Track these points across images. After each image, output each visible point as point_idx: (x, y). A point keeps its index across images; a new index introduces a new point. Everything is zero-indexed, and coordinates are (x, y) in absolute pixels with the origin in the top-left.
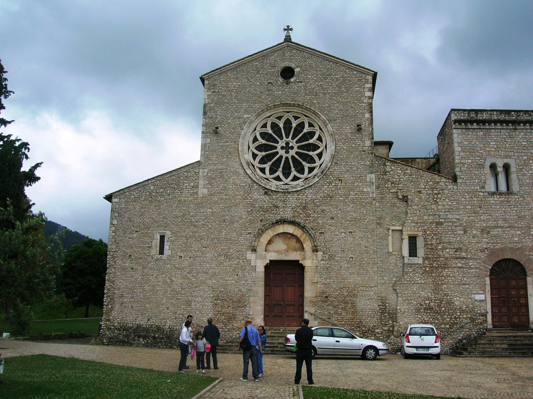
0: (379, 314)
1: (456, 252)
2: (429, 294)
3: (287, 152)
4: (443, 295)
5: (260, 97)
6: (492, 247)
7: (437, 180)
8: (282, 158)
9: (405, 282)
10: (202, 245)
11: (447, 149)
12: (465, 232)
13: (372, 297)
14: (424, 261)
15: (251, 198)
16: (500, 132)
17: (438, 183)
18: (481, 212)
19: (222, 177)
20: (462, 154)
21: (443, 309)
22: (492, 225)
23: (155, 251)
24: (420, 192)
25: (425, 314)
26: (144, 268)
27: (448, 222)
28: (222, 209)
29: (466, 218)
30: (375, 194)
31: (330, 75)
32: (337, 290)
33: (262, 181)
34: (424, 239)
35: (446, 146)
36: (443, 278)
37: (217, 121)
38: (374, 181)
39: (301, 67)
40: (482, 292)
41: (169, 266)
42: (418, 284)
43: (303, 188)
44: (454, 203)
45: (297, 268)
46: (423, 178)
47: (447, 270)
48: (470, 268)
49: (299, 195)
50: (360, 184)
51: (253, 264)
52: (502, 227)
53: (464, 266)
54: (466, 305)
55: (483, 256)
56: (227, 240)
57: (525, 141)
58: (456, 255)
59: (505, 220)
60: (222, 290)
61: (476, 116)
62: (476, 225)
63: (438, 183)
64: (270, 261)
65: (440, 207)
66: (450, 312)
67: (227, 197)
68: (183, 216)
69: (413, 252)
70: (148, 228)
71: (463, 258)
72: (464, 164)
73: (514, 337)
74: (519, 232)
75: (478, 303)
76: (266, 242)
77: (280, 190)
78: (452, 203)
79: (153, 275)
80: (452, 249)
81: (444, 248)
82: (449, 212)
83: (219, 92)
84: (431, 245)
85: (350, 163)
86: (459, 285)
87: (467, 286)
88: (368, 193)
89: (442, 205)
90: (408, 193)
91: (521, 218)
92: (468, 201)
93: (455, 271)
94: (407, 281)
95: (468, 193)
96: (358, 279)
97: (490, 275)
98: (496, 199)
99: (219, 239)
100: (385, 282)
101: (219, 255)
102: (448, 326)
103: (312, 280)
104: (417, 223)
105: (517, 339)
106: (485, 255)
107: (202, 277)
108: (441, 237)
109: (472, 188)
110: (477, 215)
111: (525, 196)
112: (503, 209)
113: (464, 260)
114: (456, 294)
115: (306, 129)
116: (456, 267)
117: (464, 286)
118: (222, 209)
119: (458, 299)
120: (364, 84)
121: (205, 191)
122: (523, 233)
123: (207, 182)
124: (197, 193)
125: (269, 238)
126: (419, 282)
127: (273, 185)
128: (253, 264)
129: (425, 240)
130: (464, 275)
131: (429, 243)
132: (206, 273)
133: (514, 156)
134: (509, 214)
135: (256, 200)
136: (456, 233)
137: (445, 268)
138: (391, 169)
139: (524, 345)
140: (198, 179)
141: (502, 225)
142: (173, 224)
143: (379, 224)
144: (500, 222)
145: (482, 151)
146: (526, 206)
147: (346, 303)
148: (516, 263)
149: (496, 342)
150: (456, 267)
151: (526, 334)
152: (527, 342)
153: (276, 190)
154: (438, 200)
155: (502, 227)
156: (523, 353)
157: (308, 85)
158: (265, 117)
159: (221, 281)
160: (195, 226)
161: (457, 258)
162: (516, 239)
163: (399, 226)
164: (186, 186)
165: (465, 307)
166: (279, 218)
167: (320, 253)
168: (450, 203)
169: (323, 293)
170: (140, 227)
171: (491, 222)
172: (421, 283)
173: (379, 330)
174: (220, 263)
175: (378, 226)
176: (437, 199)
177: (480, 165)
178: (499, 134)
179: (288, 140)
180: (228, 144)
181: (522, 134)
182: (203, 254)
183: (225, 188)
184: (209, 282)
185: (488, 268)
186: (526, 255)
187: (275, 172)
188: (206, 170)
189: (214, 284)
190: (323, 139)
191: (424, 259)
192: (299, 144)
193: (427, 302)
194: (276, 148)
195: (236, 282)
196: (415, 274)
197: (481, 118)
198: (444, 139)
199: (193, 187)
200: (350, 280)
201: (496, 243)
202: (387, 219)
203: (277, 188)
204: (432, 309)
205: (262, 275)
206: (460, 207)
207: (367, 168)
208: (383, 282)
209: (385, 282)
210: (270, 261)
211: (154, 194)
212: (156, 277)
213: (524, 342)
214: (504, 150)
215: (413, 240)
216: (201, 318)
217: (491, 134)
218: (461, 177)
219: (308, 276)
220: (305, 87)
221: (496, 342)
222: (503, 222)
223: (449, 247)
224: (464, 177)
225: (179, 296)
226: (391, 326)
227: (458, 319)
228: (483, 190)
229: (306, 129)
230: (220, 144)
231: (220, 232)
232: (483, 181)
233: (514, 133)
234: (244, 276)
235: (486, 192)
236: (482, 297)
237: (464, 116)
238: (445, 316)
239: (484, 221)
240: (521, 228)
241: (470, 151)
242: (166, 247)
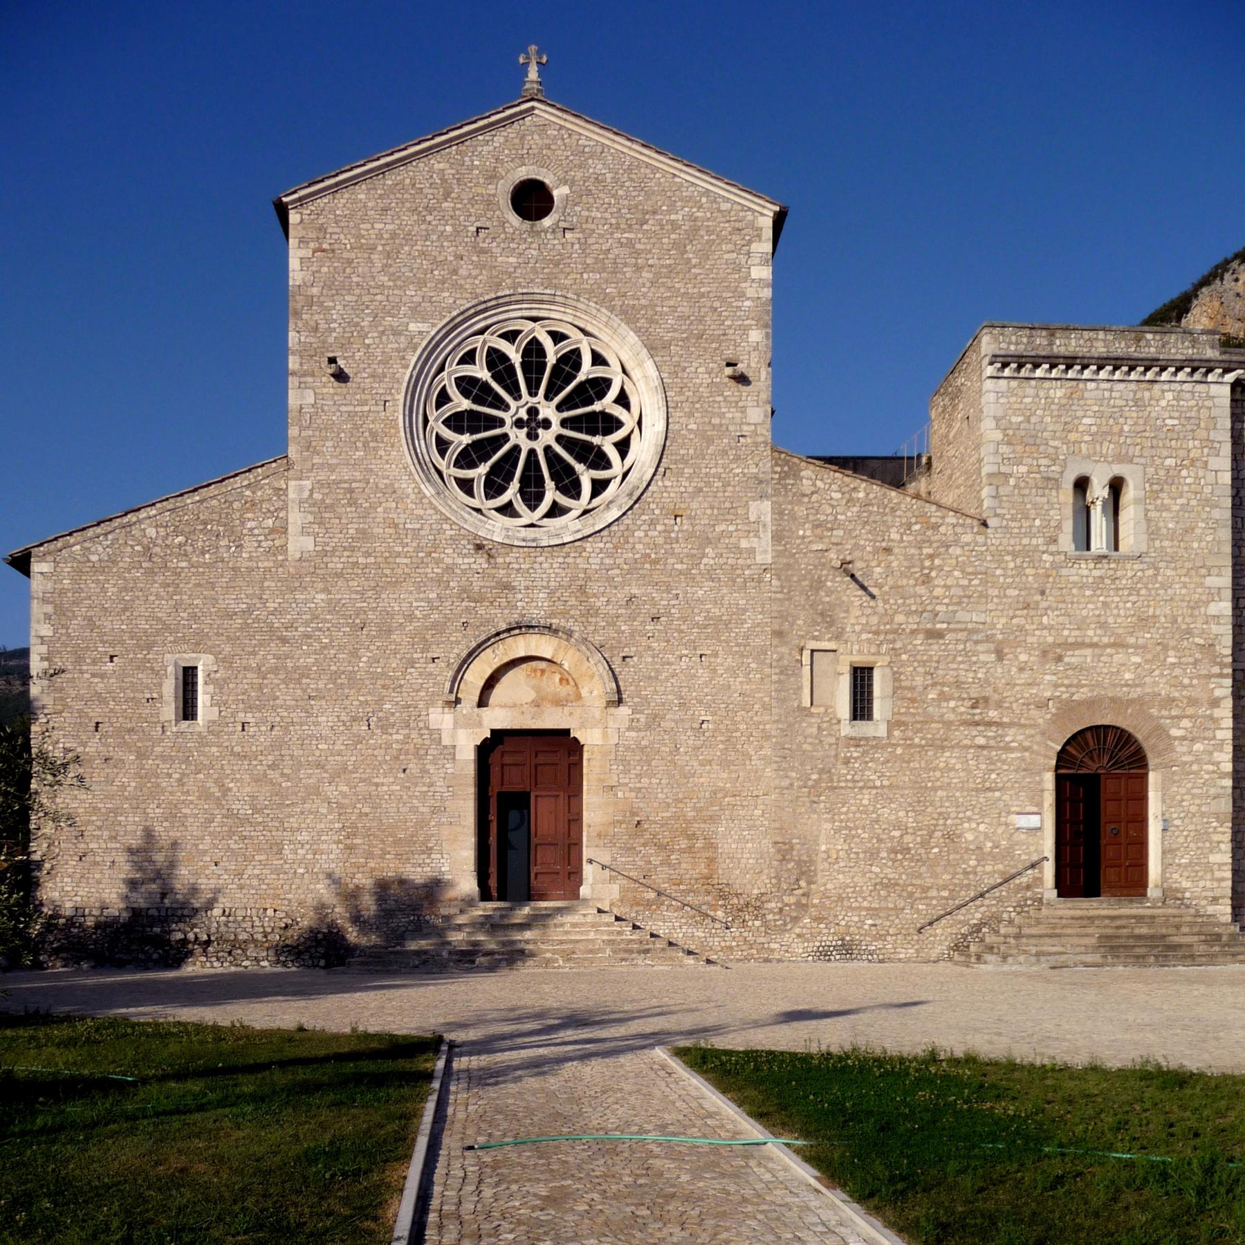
0: (775, 863)
1: (973, 707)
2: (901, 814)
3: (532, 436)
4: (936, 816)
5: (455, 272)
6: (1064, 696)
7: (933, 520)
8: (536, 455)
9: (843, 784)
10: (304, 691)
11: (960, 432)
12: (1000, 656)
13: (758, 823)
14: (889, 732)
15: (438, 562)
16: (1111, 390)
17: (936, 527)
18: (1044, 604)
19: (353, 503)
20: (1004, 449)
21: (936, 850)
22: (1071, 640)
23: (169, 709)
24: (888, 550)
25: (890, 863)
26: (141, 755)
27: (954, 630)
28: (357, 592)
29: (1003, 621)
30: (769, 556)
31: (654, 213)
32: (668, 805)
33: (466, 516)
34: (894, 673)
35: (957, 425)
36: (938, 774)
37: (331, 340)
38: (769, 519)
39: (572, 183)
40: (1035, 809)
41: (214, 749)
42: (876, 788)
43: (579, 536)
44: (975, 582)
45: (559, 749)
46: (898, 513)
47: (948, 754)
48: (1008, 749)
49: (568, 555)
50: (731, 528)
51: (446, 741)
52: (1093, 645)
53: (992, 743)
54: (993, 842)
55: (1042, 718)
56: (374, 677)
57: (1176, 414)
58: (974, 715)
59: (1103, 625)
60: (366, 810)
61: (1051, 344)
62: (1029, 639)
63: (936, 527)
64: (493, 731)
65: (938, 592)
66: (951, 857)
67: (372, 560)
68: (249, 611)
69: (861, 708)
70: (149, 647)
71: (990, 724)
72: (1007, 476)
73: (1113, 918)
74: (1137, 659)
75: (1023, 837)
76: (481, 683)
77: (516, 543)
78: (971, 580)
79: (170, 776)
80: (964, 699)
81: (943, 697)
82: (960, 603)
83: (333, 251)
84: (912, 689)
85: (704, 471)
86: (977, 790)
87: (997, 794)
88: (752, 551)
89: (945, 586)
90: (857, 554)
91: (1145, 622)
92: (1012, 576)
93: (969, 756)
94: (847, 781)
95: (1015, 555)
96: (722, 778)
97: (1057, 767)
98: (1085, 572)
99: (351, 676)
100: (792, 785)
101: (354, 719)
102: (945, 894)
103: (603, 780)
104: (877, 633)
105: (1118, 923)
106: (1049, 716)
107: (310, 777)
108: (936, 668)
109: (1025, 541)
110: (1032, 613)
111: (1162, 565)
112: (1101, 599)
113: (994, 729)
114: (969, 813)
115: (481, 372)
116: (971, 747)
117: (990, 794)
118: (357, 592)
119: (974, 825)
120: (750, 242)
121: (308, 544)
122: (1147, 661)
123: (310, 518)
124: (283, 549)
125: (489, 672)
126: (878, 783)
127: (497, 528)
128: (446, 741)
129: (896, 677)
130: (992, 767)
131: (903, 684)
132: (319, 765)
133: (1141, 456)
134: (1115, 611)
135: (450, 569)
136: (974, 659)
137: (943, 748)
138: (813, 489)
139: (1140, 937)
140: (285, 508)
141: (1095, 639)
142: (217, 634)
143: (779, 634)
144: (1090, 633)
145: (1056, 443)
146: (1162, 592)
147: (692, 837)
148: (1099, 731)
149: (1069, 931)
150: (971, 747)
151: (1141, 912)
152: (1144, 931)
153: (507, 541)
154: (933, 574)
155: (1093, 645)
156: (1138, 957)
157: (591, 241)
158: (582, 325)
159: (362, 787)
160: (284, 640)
161: (977, 724)
162: (1127, 676)
163: (829, 640)
164: (251, 529)
165: (989, 844)
166: (515, 617)
167: (624, 711)
168: (966, 582)
169: (633, 814)
170: (122, 643)
171: (1066, 633)
172: (882, 787)
173: (773, 905)
174: (359, 740)
175: (775, 641)
176: (931, 569)
177: (1049, 479)
178: (1107, 394)
179: (535, 400)
180: (366, 408)
181: (1169, 396)
182: (309, 715)
183: (363, 535)
184: (330, 790)
185: (1052, 748)
186: (1151, 716)
187: (501, 490)
188: (307, 484)
189: (345, 795)
190: (634, 401)
191: (892, 725)
192: (566, 414)
193: (897, 834)
194: (501, 423)
195: (403, 787)
196: (867, 763)
197: (1063, 349)
198: (954, 407)
199: (272, 531)
200: (702, 780)
201: (1077, 686)
202: (800, 622)
203: (508, 537)
204: (909, 849)
205: (470, 770)
206: (990, 592)
207: (751, 483)
208: (786, 783)
209: (792, 785)
210: (493, 731)
211: (157, 550)
212: (180, 780)
213: (1137, 931)
214: (1115, 438)
215: (861, 678)
216: (312, 887)
217: (1086, 395)
218: (999, 511)
219: (592, 770)
220: (584, 245)
221: (1069, 931)
222: (1099, 632)
223: (956, 695)
224: (1004, 511)
225: (247, 830)
226: (804, 895)
227: (971, 876)
228: (1053, 548)
229: (481, 372)
230: (344, 409)
231: (355, 654)
232: (1053, 524)
233: (1147, 394)
234: (424, 771)
235: (1059, 553)
236: (1034, 821)
237: (1017, 344)
238: (939, 870)
239: (1050, 628)
240: (1144, 647)
241: (1023, 440)
242: (202, 699)
